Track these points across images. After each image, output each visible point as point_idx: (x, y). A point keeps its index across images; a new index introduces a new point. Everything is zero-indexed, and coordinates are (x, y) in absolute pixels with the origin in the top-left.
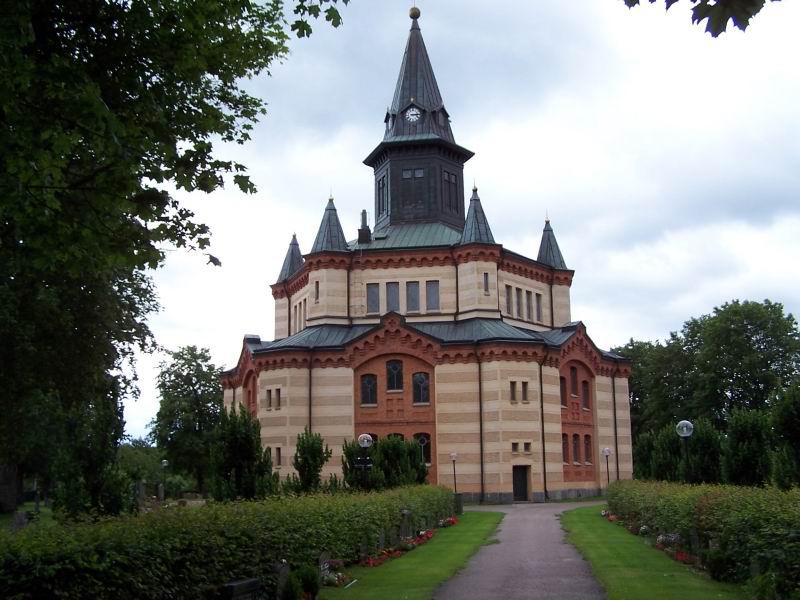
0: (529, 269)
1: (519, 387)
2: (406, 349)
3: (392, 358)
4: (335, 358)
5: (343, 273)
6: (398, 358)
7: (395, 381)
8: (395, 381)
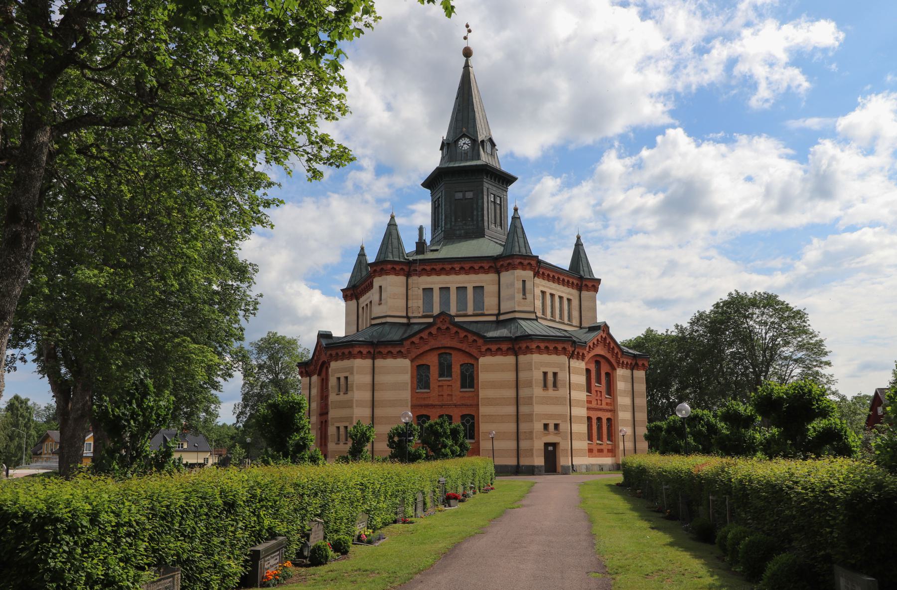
0: (428, 268)
1: (550, 377)
3: (443, 351)
4: (395, 350)
5: (402, 279)
8: (445, 370)
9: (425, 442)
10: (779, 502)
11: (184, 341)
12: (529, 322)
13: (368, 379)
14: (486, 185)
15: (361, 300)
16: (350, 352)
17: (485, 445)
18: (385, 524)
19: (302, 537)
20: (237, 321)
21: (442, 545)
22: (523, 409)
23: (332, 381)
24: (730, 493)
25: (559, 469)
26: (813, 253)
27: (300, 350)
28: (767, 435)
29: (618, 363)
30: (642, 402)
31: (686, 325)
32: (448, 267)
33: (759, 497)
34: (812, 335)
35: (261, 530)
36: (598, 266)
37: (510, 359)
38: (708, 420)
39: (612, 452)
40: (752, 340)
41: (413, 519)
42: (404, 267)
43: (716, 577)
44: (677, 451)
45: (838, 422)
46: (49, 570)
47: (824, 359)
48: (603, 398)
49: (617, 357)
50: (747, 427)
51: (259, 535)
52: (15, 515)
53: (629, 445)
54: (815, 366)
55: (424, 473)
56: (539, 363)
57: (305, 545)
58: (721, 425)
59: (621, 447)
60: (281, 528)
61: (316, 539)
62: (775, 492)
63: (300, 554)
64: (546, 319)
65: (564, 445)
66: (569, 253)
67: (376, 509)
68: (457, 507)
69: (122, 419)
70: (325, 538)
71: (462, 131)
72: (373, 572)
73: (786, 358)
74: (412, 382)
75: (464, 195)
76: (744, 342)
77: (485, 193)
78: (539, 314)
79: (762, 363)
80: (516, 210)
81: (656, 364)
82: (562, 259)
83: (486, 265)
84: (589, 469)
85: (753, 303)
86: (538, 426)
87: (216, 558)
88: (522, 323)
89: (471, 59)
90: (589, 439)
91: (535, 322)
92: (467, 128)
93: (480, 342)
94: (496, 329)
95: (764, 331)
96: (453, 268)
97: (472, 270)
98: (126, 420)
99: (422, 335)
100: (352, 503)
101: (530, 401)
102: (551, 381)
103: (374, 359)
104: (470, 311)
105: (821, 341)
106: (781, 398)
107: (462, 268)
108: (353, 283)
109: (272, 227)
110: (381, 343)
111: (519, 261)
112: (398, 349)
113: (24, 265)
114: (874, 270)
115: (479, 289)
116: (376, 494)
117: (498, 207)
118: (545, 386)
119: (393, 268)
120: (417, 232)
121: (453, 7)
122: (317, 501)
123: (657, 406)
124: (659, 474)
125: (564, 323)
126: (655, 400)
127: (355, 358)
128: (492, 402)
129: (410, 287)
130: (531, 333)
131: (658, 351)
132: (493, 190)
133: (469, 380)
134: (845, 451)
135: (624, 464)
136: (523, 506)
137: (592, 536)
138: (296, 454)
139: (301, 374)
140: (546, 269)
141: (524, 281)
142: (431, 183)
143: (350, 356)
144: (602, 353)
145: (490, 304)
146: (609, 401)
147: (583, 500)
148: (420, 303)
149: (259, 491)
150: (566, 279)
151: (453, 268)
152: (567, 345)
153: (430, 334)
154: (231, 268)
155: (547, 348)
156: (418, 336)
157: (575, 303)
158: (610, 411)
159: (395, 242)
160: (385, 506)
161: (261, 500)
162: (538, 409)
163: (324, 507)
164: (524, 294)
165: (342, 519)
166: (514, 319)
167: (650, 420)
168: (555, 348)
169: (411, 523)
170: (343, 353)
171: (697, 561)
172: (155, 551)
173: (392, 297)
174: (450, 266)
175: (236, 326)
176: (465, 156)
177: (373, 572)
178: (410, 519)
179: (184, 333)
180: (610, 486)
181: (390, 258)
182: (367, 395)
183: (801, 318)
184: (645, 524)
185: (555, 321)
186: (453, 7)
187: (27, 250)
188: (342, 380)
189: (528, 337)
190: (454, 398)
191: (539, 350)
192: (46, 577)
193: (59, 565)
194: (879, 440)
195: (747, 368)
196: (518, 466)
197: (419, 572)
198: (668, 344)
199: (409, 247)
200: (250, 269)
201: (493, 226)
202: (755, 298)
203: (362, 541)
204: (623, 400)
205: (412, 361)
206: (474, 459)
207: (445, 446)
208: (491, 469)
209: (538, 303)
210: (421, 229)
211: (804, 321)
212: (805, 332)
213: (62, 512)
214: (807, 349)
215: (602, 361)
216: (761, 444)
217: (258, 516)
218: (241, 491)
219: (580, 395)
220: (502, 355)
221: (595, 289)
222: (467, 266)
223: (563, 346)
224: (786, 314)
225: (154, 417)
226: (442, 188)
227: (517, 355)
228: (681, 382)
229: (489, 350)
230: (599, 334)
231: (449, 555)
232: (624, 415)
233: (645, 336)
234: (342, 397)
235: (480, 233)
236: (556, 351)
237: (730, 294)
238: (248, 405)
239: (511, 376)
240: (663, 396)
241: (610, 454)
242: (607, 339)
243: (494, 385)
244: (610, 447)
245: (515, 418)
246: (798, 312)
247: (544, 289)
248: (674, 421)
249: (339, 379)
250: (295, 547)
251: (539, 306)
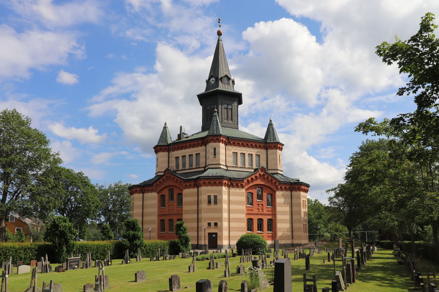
0: (176, 147)
1: (212, 198)
3: (170, 188)
4: (150, 188)
5: (166, 153)
7: (172, 198)
8: (172, 198)
42: (166, 148)
48: (264, 208)
86: (206, 225)
89: (222, 37)
104: (187, 166)
111: (211, 138)
112: (152, 188)
115: (198, 155)
119: (161, 149)
145: (202, 161)
205: (158, 193)
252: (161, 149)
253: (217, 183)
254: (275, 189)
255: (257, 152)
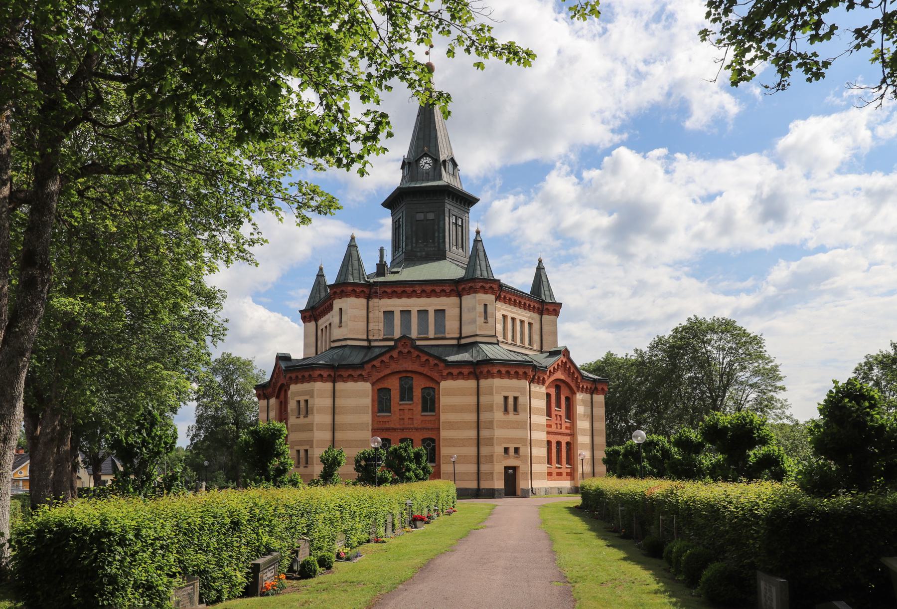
0: (389, 290)
1: (511, 401)
2: (416, 367)
3: (404, 375)
4: (356, 373)
5: (362, 301)
6: (409, 375)
7: (406, 393)
8: (406, 393)
9: (389, 466)
10: (716, 520)
11: (156, 367)
12: (490, 346)
13: (328, 402)
14: (448, 206)
15: (320, 322)
16: (310, 375)
17: (445, 468)
18: (360, 543)
19: (292, 553)
20: (205, 347)
21: (418, 561)
22: (484, 433)
23: (292, 405)
24: (677, 513)
25: (519, 492)
26: (781, 272)
27: (255, 372)
28: (714, 460)
29: (578, 387)
30: (601, 426)
31: (645, 348)
32: (409, 289)
33: (701, 516)
34: (768, 360)
35: (259, 546)
36: (560, 287)
37: (472, 384)
38: (663, 446)
39: (572, 475)
40: (710, 365)
41: (384, 539)
42: (365, 289)
43: (661, 584)
44: (633, 474)
45: (776, 448)
46: (105, 575)
47: (779, 384)
48: (563, 422)
49: (577, 382)
50: (698, 452)
51: (258, 550)
52: (75, 530)
53: (588, 469)
54: (770, 391)
55: (392, 496)
56: (499, 387)
57: (295, 560)
58: (674, 450)
59: (580, 471)
60: (276, 544)
61: (303, 557)
62: (713, 511)
63: (291, 569)
64: (507, 343)
65: (523, 468)
66: (530, 280)
67: (352, 529)
68: (423, 528)
69: (135, 446)
70: (310, 555)
71: (423, 150)
72: (359, 583)
73: (742, 383)
74: (373, 405)
75: (425, 216)
76: (702, 366)
77: (447, 214)
78: (500, 338)
79: (719, 387)
80: (478, 233)
81: (616, 388)
82: (521, 280)
83: (448, 289)
84: (547, 491)
85: (712, 329)
86: (499, 450)
87: (226, 569)
88: (483, 346)
90: (548, 463)
91: (496, 346)
92: (429, 147)
93: (442, 365)
94: (458, 353)
95: (721, 356)
96: (414, 291)
97: (433, 294)
98: (139, 448)
99: (383, 358)
100: (332, 523)
101: (490, 425)
102: (512, 405)
103: (334, 382)
104: (431, 334)
105: (777, 366)
106: (726, 427)
107: (423, 291)
108: (312, 305)
109: (257, 265)
110: (342, 367)
111: (481, 284)
112: (359, 373)
113: (39, 305)
114: (839, 293)
115: (440, 313)
116: (353, 515)
117: (460, 229)
118: (506, 410)
119: (354, 290)
120: (378, 254)
121: (449, 112)
122: (304, 521)
123: (616, 430)
124: (616, 496)
125: (524, 347)
126: (614, 424)
127: (315, 381)
128: (452, 426)
129: (370, 309)
130: (492, 357)
131: (617, 375)
132: (455, 211)
133: (430, 403)
134: (779, 475)
135: (582, 488)
136: (488, 527)
137: (553, 552)
138: (277, 477)
139: (258, 396)
140: (508, 292)
141: (486, 305)
142: (394, 202)
143: (311, 379)
144: (563, 377)
145: (451, 327)
146: (568, 425)
147: (544, 521)
148: (381, 326)
149: (257, 511)
150: (527, 303)
151: (414, 291)
152: (527, 371)
153: (391, 357)
154: (199, 294)
155: (508, 372)
156: (379, 359)
157: (536, 327)
158: (569, 435)
159: (356, 263)
160: (360, 526)
161: (259, 520)
162: (499, 433)
163: (309, 526)
164: (486, 318)
165: (324, 537)
166: (475, 344)
167: (609, 444)
168: (516, 373)
169: (383, 542)
170: (303, 376)
171: (646, 572)
172: (180, 562)
173: (352, 320)
174: (411, 289)
175: (204, 351)
176: (427, 176)
177: (359, 583)
178: (382, 539)
179: (155, 359)
180: (569, 508)
181: (351, 280)
182: (328, 419)
183: (758, 343)
184: (602, 543)
185: (516, 345)
186: (449, 112)
187: (42, 291)
188: (302, 404)
189: (489, 362)
190: (415, 422)
191: (500, 375)
192: (105, 580)
193: (114, 571)
194: (801, 466)
195: (703, 393)
196: (478, 489)
197: (401, 582)
198: (628, 369)
199: (370, 267)
200: (219, 295)
201: (454, 248)
202: (713, 324)
203: (341, 558)
204: (583, 424)
205: (373, 384)
206: (436, 482)
207: (409, 470)
208: (453, 492)
209: (499, 327)
210: (382, 251)
211: (760, 347)
212: (762, 358)
213: (112, 527)
214: (763, 374)
215: (562, 385)
216: (708, 468)
217: (257, 534)
218: (244, 511)
219: (540, 419)
220: (463, 379)
221: (556, 313)
222: (428, 289)
223: (524, 370)
224: (744, 339)
225: (163, 445)
226: (404, 208)
227: (478, 380)
228: (639, 406)
229: (450, 374)
230: (561, 358)
231: (424, 569)
232: (583, 439)
233: (606, 360)
234: (302, 420)
235: (440, 255)
236: (517, 376)
237: (689, 319)
238: (202, 427)
239: (473, 400)
240: (621, 419)
241: (569, 477)
242: (568, 365)
243: (454, 409)
244: (569, 471)
245: (476, 442)
246: (755, 338)
247: (505, 313)
248: (631, 446)
249: (299, 402)
250: (286, 562)
251: (503, 331)
252: (354, 290)
253: (512, 372)
254: (575, 389)
255: (529, 317)
